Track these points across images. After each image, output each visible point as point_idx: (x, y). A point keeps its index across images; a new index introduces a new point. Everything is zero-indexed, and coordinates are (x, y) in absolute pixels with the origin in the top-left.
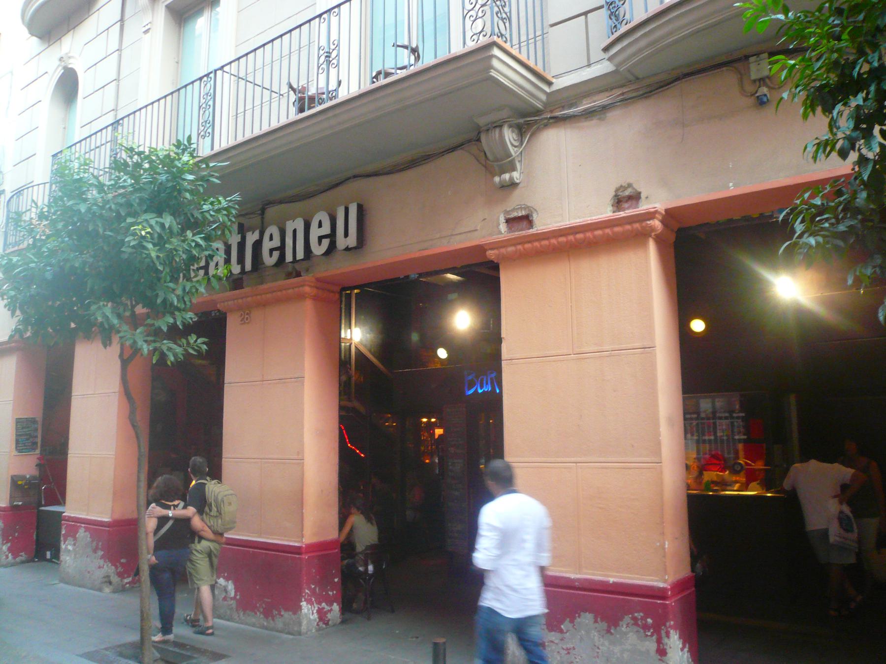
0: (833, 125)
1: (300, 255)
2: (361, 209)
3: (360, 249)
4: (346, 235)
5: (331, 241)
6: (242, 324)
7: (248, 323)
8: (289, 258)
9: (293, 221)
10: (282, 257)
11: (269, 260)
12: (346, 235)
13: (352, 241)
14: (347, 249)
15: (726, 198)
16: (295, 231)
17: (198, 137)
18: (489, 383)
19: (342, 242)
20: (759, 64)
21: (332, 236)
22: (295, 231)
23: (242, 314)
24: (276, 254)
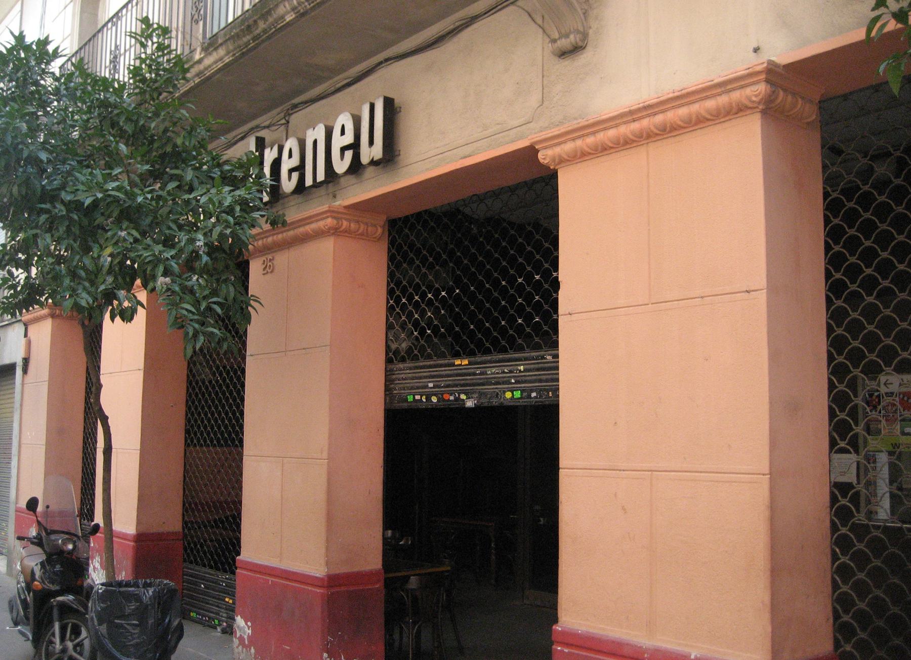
0: (266, 240)
1: (321, 177)
2: (389, 104)
3: (317, 189)
4: (371, 142)
5: (354, 152)
6: (264, 274)
7: (272, 272)
8: (309, 182)
9: (314, 129)
10: (356, 157)
11: (288, 184)
12: (371, 142)
13: (377, 151)
14: (373, 163)
15: (767, 242)
16: (315, 142)
17: (192, 23)
18: (332, 590)
19: (368, 153)
20: (756, 50)
21: (355, 146)
22: (315, 142)
23: (264, 261)
24: (349, 154)
